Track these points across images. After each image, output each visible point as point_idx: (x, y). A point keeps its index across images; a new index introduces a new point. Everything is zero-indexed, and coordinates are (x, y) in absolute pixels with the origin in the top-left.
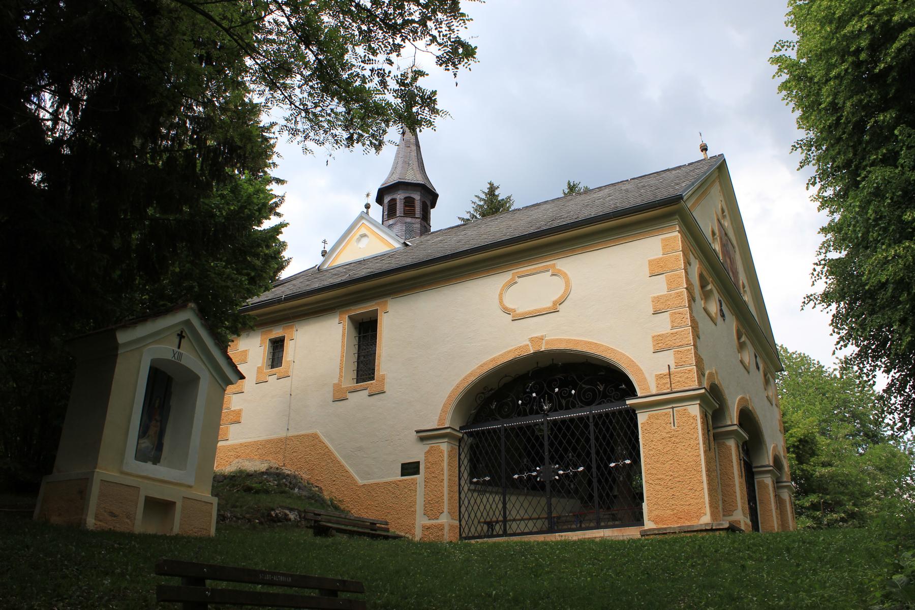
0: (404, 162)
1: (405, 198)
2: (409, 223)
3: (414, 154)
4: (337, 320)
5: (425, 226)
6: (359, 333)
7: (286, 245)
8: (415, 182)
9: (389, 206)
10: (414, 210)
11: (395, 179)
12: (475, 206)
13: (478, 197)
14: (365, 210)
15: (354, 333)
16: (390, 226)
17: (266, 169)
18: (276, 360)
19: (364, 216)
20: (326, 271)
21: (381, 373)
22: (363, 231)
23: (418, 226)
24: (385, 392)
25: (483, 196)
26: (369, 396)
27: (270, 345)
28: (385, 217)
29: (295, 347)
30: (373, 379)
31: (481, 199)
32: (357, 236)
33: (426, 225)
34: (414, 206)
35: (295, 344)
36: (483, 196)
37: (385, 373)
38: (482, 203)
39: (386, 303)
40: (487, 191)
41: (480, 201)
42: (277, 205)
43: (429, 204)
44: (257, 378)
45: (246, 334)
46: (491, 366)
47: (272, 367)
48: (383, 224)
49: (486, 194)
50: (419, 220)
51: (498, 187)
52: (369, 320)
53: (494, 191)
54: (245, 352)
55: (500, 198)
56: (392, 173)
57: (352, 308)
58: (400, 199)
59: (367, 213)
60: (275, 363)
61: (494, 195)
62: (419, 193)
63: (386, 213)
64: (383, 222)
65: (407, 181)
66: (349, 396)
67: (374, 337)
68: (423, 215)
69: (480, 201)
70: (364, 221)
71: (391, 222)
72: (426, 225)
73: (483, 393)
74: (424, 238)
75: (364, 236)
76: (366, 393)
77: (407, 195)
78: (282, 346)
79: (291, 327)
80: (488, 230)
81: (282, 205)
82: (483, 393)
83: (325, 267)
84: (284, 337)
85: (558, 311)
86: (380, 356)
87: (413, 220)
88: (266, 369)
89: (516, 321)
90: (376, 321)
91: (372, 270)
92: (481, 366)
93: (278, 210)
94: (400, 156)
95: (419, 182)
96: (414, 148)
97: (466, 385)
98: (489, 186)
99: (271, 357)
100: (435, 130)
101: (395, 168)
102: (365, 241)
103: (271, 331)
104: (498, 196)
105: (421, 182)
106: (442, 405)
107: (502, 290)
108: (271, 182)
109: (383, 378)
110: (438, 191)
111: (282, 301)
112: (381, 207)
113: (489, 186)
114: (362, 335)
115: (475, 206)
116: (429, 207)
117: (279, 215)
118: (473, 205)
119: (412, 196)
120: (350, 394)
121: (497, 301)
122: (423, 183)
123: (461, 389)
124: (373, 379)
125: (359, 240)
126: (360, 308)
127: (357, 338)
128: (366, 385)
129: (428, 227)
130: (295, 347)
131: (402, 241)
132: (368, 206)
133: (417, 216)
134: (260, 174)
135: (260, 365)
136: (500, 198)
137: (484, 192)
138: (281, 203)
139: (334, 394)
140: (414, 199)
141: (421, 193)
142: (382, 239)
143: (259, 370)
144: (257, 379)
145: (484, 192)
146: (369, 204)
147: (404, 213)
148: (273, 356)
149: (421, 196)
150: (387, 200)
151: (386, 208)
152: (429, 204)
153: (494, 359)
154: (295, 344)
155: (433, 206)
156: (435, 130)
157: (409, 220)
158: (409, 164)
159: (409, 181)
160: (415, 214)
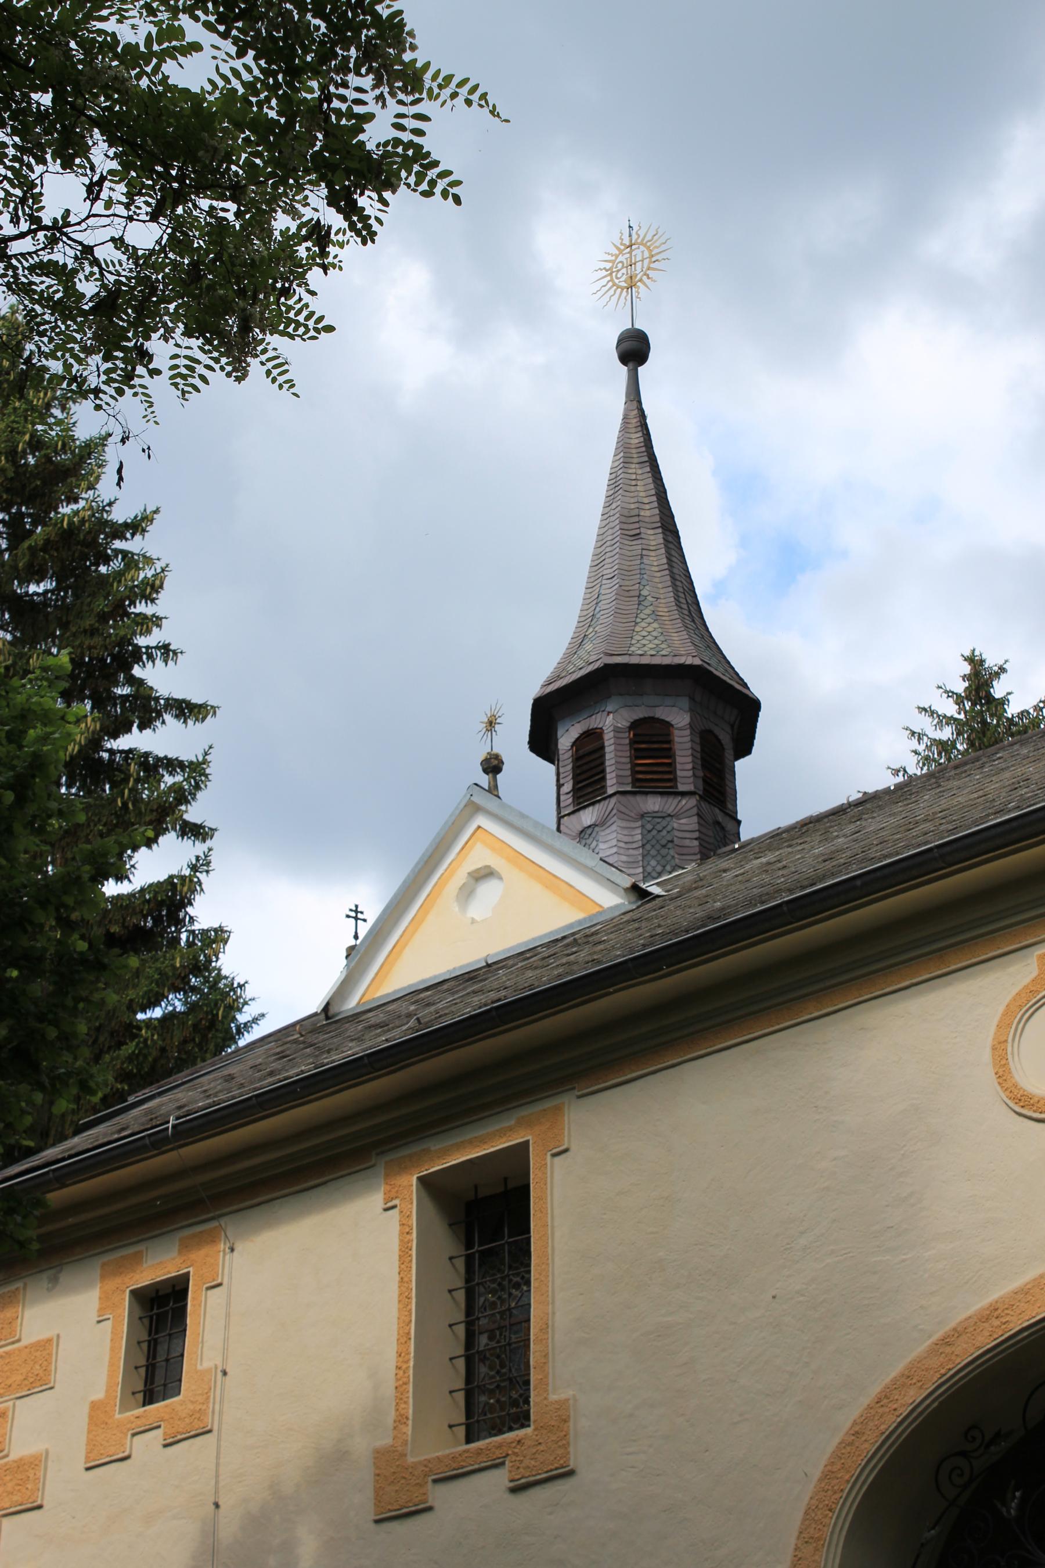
0: (623, 593)
1: (635, 725)
2: (654, 815)
3: (657, 559)
4: (376, 1199)
5: (718, 823)
6: (469, 1245)
7: (225, 941)
8: (667, 661)
9: (577, 759)
10: (672, 765)
11: (591, 658)
12: (921, 748)
13: (931, 712)
14: (484, 780)
15: (447, 1244)
16: (584, 835)
17: (137, 671)
18: (160, 1374)
19: (481, 799)
20: (355, 1017)
21: (553, 1397)
22: (480, 856)
23: (690, 823)
24: (571, 1473)
25: (949, 708)
26: (514, 1490)
27: (138, 1313)
28: (567, 800)
29: (228, 1315)
30: (522, 1419)
31: (944, 720)
32: (460, 877)
33: (720, 817)
34: (669, 753)
35: (229, 1304)
36: (949, 708)
37: (570, 1393)
38: (946, 734)
39: (558, 1110)
40: (960, 687)
41: (940, 725)
42: (182, 796)
43: (725, 738)
44: (92, 1445)
45: (45, 1276)
46: (985, 1340)
47: (149, 1398)
48: (559, 830)
49: (959, 700)
50: (690, 802)
51: (1003, 670)
52: (501, 1189)
53: (988, 684)
54: (45, 1348)
55: (1012, 710)
56: (579, 641)
57: (434, 1145)
58: (617, 730)
59: (493, 790)
60: (159, 1380)
61: (990, 699)
62: (685, 702)
63: (568, 787)
64: (560, 818)
65: (634, 660)
66: (440, 1496)
67: (522, 1254)
68: (705, 781)
69: (940, 725)
70: (481, 820)
71: (588, 817)
72: (720, 817)
73: (963, 1454)
74: (714, 864)
75: (484, 874)
76: (501, 1478)
77: (640, 713)
78: (181, 1314)
79: (211, 1238)
80: (944, 803)
81: (200, 795)
82: (963, 1454)
83: (352, 1004)
84: (186, 1277)
85: (566, 1151)
86: (544, 1329)
87: (671, 804)
88: (124, 1409)
89: (45, 1393)
90: (522, 1193)
91: (503, 993)
92: (946, 1341)
93: (193, 813)
94: (608, 572)
95: (681, 660)
96: (655, 538)
97: (890, 1422)
98: (967, 669)
99: (143, 1361)
100: (457, 200)
101: (588, 619)
102: (489, 892)
103: (137, 1259)
104: (1003, 702)
105: (689, 661)
106: (799, 1516)
107: (1003, 1025)
108: (159, 714)
109: (563, 1416)
110: (757, 689)
111: (166, 1140)
112: (550, 769)
113: (967, 669)
114: (155, 1311)
115: (921, 748)
116: (729, 753)
117: (196, 832)
118: (914, 744)
119: (661, 713)
120: (443, 1489)
121: (987, 1074)
122: (697, 662)
123: (869, 1444)
124: (522, 1419)
125: (466, 893)
126: (471, 1142)
127: (460, 1263)
128: (500, 1446)
129: (729, 825)
130: (228, 1315)
131: (627, 882)
132: (493, 766)
133: (681, 788)
134: (119, 691)
135: (99, 1395)
136: (1012, 710)
137: (950, 694)
138: (197, 787)
139: (378, 1492)
140: (668, 725)
141: (692, 699)
142: (552, 882)
143: (97, 1412)
144: (89, 1452)
145: (950, 694)
146: (497, 757)
147: (635, 781)
148: (152, 1353)
149: (691, 710)
150: (567, 738)
151: (567, 768)
152: (725, 738)
153: (993, 1311)
154: (229, 1304)
155: (744, 746)
156: (457, 200)
157: (653, 804)
158: (640, 599)
159: (645, 661)
160: (674, 780)
